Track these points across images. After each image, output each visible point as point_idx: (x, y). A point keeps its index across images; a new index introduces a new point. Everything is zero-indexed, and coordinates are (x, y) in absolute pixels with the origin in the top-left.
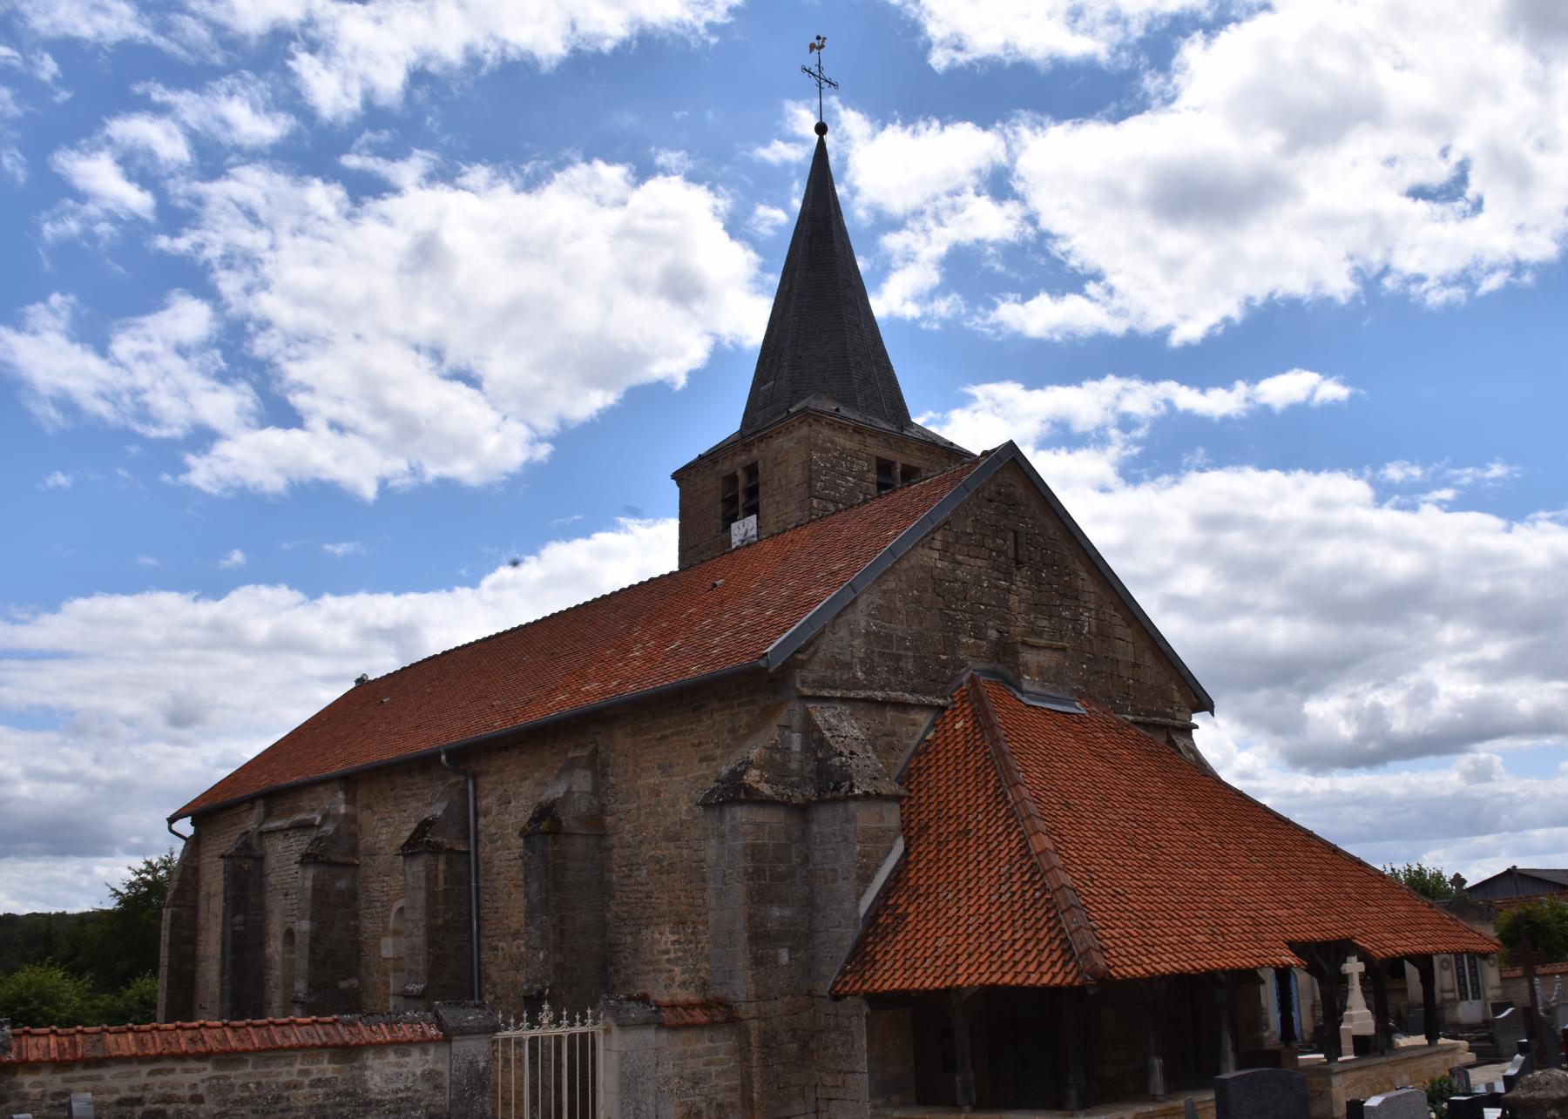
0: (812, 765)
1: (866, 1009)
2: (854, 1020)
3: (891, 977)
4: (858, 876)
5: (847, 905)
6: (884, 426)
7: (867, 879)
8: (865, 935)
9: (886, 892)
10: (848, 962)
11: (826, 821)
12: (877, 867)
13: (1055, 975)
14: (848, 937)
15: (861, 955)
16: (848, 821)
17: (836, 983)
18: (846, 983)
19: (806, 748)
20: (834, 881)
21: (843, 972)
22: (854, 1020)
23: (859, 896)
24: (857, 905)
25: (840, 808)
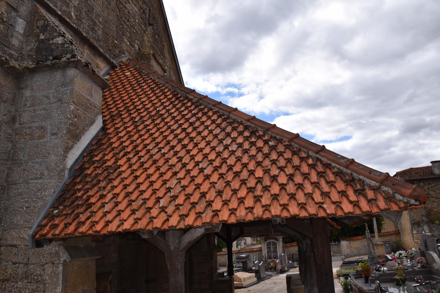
0: (33, 45)
1: (64, 256)
2: (49, 269)
3: (113, 216)
4: (69, 131)
5: (53, 157)
6: (73, 14)
7: (76, 137)
8: (72, 183)
9: (89, 153)
10: (54, 207)
11: (41, 86)
12: (84, 131)
13: (136, 221)
14: (52, 188)
15: (69, 198)
16: (64, 85)
17: (41, 227)
18: (55, 226)
19: (29, 32)
20: (41, 137)
21: (50, 216)
22: (49, 269)
23: (68, 149)
24: (65, 157)
25: (58, 75)
